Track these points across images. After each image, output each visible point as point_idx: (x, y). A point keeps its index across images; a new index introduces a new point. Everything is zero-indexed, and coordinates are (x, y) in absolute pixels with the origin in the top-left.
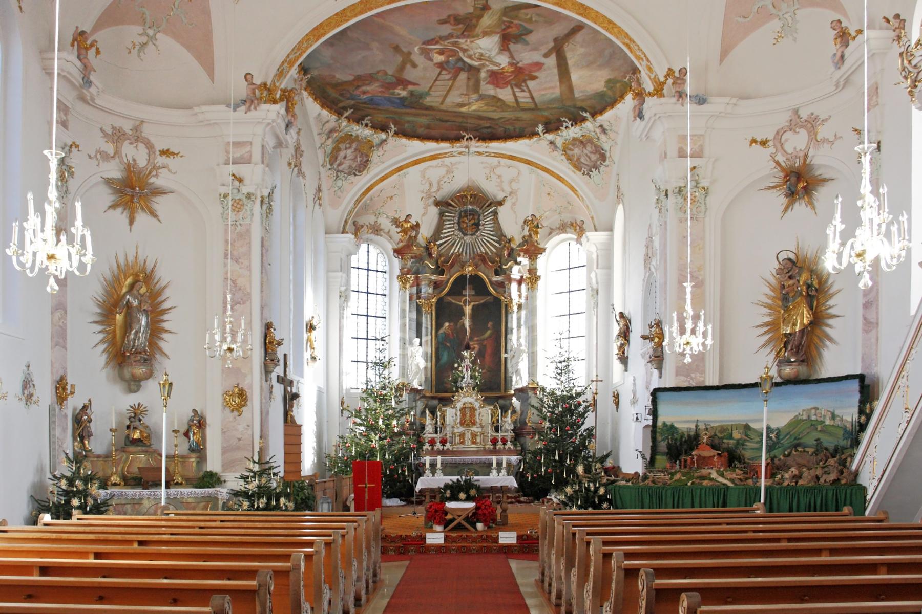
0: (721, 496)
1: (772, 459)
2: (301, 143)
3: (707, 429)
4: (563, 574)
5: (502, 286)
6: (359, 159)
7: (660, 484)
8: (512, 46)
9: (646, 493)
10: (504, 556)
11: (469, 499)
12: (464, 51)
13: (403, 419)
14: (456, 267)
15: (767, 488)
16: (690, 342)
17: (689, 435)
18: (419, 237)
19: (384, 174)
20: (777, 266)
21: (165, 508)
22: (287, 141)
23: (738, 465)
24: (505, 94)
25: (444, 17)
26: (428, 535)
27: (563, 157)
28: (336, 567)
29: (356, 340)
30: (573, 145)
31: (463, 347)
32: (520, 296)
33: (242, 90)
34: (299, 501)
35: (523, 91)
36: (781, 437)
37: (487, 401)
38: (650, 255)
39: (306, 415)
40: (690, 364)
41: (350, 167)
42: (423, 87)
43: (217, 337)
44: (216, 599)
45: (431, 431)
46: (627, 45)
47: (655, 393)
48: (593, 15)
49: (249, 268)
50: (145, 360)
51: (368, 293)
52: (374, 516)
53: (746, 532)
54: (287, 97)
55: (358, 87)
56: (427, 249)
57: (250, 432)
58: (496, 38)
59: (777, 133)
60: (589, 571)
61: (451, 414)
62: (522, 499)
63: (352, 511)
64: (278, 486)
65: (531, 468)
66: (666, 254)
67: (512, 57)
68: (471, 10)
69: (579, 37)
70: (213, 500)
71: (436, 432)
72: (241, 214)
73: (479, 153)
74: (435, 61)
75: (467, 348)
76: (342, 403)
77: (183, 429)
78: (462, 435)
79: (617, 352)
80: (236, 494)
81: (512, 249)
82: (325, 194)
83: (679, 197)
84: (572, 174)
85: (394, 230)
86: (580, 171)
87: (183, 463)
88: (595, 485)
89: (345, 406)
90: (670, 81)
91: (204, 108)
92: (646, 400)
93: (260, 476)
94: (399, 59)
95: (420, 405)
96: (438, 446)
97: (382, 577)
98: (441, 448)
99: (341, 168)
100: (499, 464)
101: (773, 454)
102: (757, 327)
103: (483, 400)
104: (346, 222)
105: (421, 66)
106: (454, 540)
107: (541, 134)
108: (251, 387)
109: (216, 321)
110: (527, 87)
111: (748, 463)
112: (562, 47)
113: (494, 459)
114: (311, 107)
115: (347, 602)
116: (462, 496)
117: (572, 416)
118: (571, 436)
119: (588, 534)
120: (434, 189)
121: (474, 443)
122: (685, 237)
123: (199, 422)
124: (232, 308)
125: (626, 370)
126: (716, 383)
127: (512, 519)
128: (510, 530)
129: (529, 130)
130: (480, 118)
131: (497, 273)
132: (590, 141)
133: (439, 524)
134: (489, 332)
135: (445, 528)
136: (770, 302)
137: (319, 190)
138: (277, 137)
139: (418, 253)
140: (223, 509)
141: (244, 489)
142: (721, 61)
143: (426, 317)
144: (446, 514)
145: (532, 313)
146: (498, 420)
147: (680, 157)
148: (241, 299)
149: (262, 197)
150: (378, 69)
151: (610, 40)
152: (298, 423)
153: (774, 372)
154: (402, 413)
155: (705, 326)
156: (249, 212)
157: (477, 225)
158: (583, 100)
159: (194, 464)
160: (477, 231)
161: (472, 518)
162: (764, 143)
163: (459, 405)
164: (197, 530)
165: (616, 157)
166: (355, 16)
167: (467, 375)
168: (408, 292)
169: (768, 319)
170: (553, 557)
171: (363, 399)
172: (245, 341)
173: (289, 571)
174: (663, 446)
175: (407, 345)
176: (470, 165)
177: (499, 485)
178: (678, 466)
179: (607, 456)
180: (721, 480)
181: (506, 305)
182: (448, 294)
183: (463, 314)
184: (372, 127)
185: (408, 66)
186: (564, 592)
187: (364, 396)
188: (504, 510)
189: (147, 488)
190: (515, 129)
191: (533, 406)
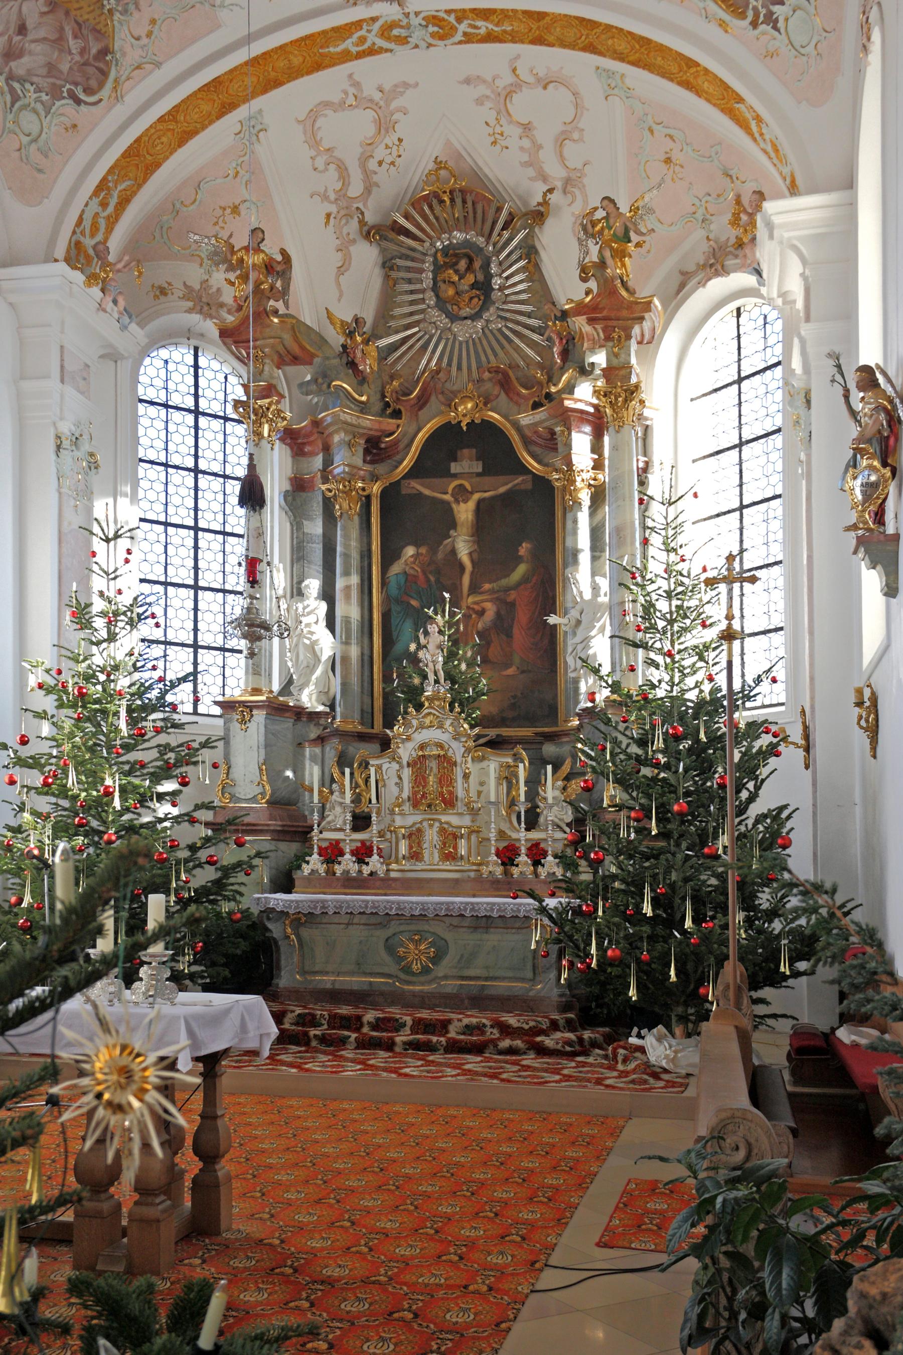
5: (553, 444)
6: (74, 45)
14: (434, 403)
61: (392, 776)
78: (415, 835)
84: (713, 32)
86: (742, 16)
96: (347, 864)
120: (356, 189)
157: (484, 288)
163: (406, 752)
182: (413, 473)
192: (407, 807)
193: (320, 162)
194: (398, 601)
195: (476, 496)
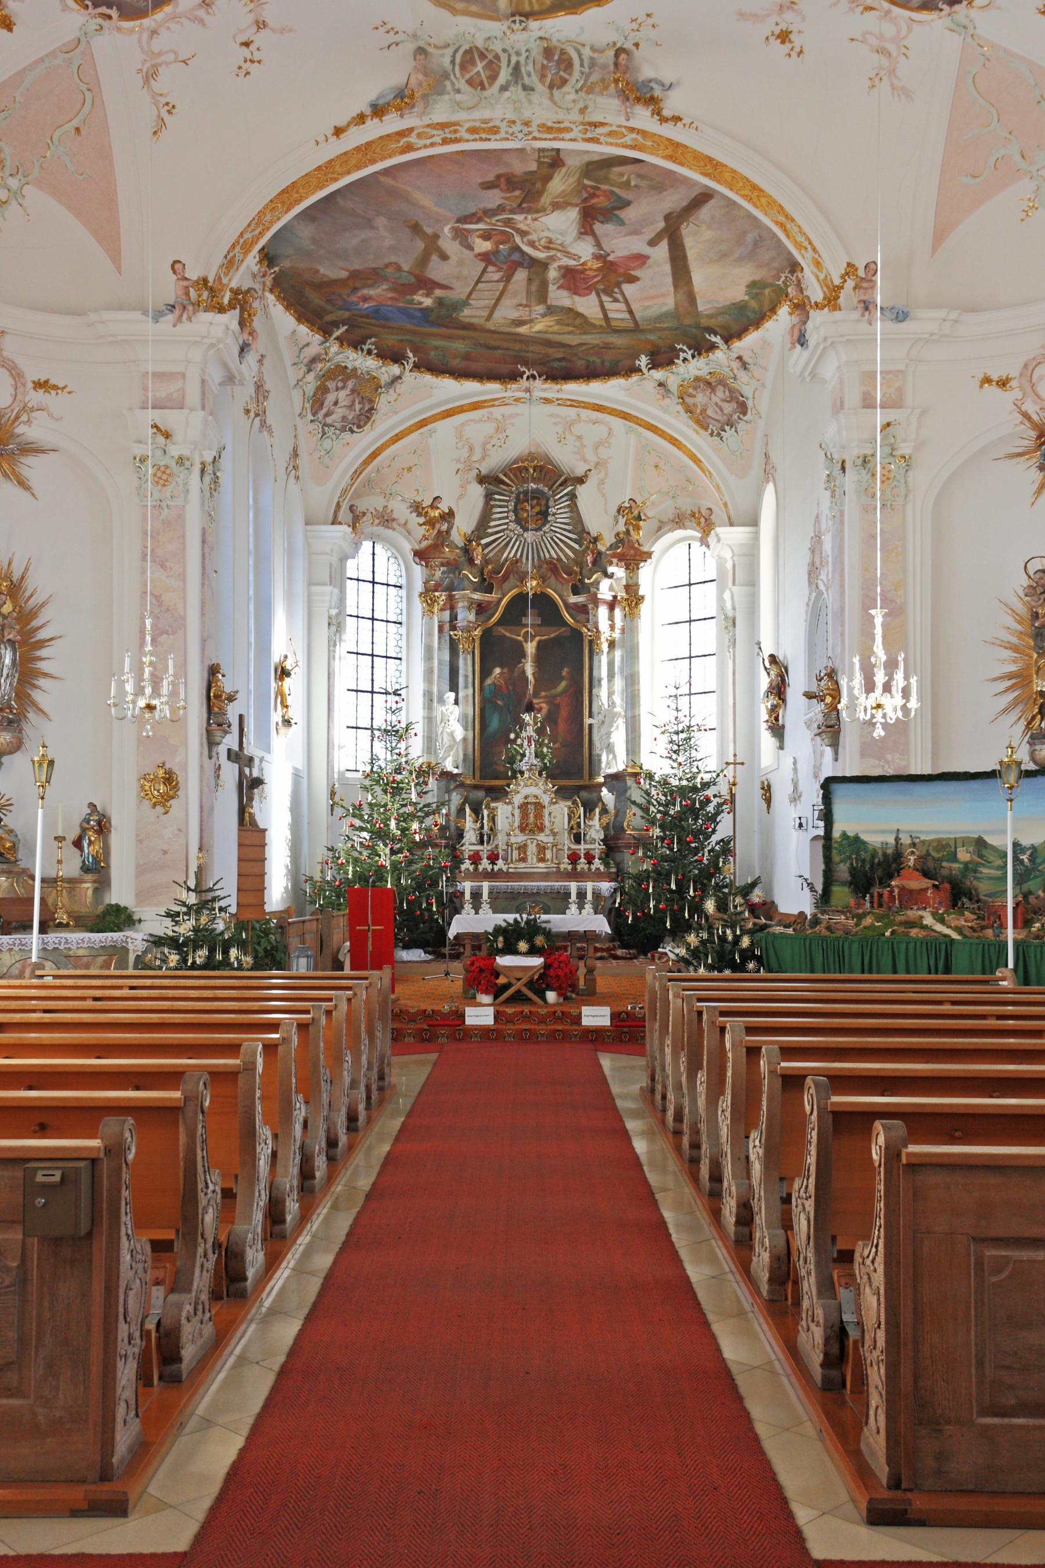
0: (941, 957)
1: (1026, 896)
2: (266, 378)
3: (914, 845)
4: (684, 1079)
5: (582, 611)
7: (839, 933)
8: (598, 227)
9: (819, 949)
10: (591, 1046)
11: (533, 951)
12: (523, 234)
13: (429, 821)
14: (512, 580)
15: (1017, 944)
16: (879, 704)
17: (885, 855)
18: (454, 532)
19: (397, 431)
20: (1025, 582)
21: (39, 966)
22: (241, 373)
23: (968, 904)
24: (588, 305)
25: (491, 177)
26: (469, 1011)
27: (680, 408)
28: (316, 1065)
29: (356, 694)
30: (695, 389)
31: (524, 707)
32: (612, 627)
33: (169, 289)
34: (261, 953)
35: (616, 300)
36: (1039, 861)
37: (563, 793)
38: (818, 564)
39: (275, 814)
40: (882, 739)
41: (344, 418)
42: (459, 292)
43: (129, 688)
44: (110, 1125)
45: (474, 840)
46: (782, 225)
47: (828, 785)
48: (727, 176)
49: (182, 577)
50: (10, 722)
51: (373, 619)
52: (379, 978)
53: (983, 1017)
54: (241, 302)
55: (355, 289)
56: (467, 551)
57: (182, 841)
58: (572, 216)
59: (1026, 366)
60: (725, 1075)
61: (505, 814)
62: (619, 952)
63: (347, 971)
64: (227, 929)
65: (632, 901)
66: (842, 563)
67: (598, 245)
68: (533, 167)
69: (705, 212)
70: (119, 953)
71: (482, 843)
72: (168, 490)
73: (547, 401)
74: (477, 250)
75: (530, 708)
76: (333, 794)
77: (73, 834)
78: (523, 848)
79: (766, 717)
80: (158, 941)
81: (600, 553)
82: (304, 461)
83: (864, 472)
85: (415, 520)
86: (706, 429)
87: (71, 891)
88: (734, 932)
89: (337, 799)
90: (850, 284)
91: (106, 315)
92: (813, 796)
93: (198, 912)
94: (420, 245)
95: (456, 799)
96: (485, 864)
97: (394, 1080)
98: (489, 867)
99: (329, 420)
100: (581, 895)
101: (1026, 887)
102: (995, 680)
103: (556, 792)
104: (338, 506)
105: (454, 259)
106: (510, 1019)
107: (645, 370)
108: (185, 766)
109: (127, 661)
110: (623, 294)
111: (985, 902)
112: (678, 228)
113: (573, 887)
114: (279, 319)
115: (335, 1124)
116: (523, 946)
117: (696, 819)
118: (696, 851)
119: (724, 1013)
120: (477, 456)
121: (542, 860)
122: (874, 536)
123: (99, 823)
124: (153, 640)
125: (781, 747)
126: (927, 770)
127: (602, 984)
128: (599, 1004)
129: (626, 363)
130: (549, 343)
131: (576, 591)
132: (722, 382)
133: (486, 992)
134: (563, 684)
135: (495, 999)
136: (1014, 640)
137: (295, 454)
138: (225, 366)
139: (452, 556)
140: (135, 968)
141: (171, 934)
142: (934, 249)
143: (465, 659)
144: (497, 975)
145: (632, 654)
146: (579, 824)
147: (865, 407)
148: (168, 626)
149: (203, 463)
150: (387, 261)
151: (755, 218)
152: (262, 826)
153: (1023, 755)
154: (428, 811)
155: (906, 678)
156: (181, 487)
157: (544, 515)
158: (711, 316)
159: (90, 892)
160: (544, 525)
161: (540, 983)
162: (1003, 383)
163: (518, 800)
164: (90, 1004)
165: (763, 406)
166: (349, 173)
167: (530, 751)
168: (436, 618)
169: (1013, 668)
170: (668, 1051)
171: (365, 788)
172: (174, 694)
173: (237, 1073)
174: (843, 870)
175: (435, 704)
176: (531, 419)
177: (581, 928)
178: (868, 905)
179: (754, 885)
180: (939, 928)
181: (591, 642)
183: (523, 654)
184: (378, 355)
185: (434, 258)
186: (686, 1111)
187: (367, 783)
188: (590, 971)
189: (10, 934)
190: (603, 362)
191: (634, 803)
192: (517, 831)
193: (460, 445)
194: (490, 701)
195: (537, 638)
